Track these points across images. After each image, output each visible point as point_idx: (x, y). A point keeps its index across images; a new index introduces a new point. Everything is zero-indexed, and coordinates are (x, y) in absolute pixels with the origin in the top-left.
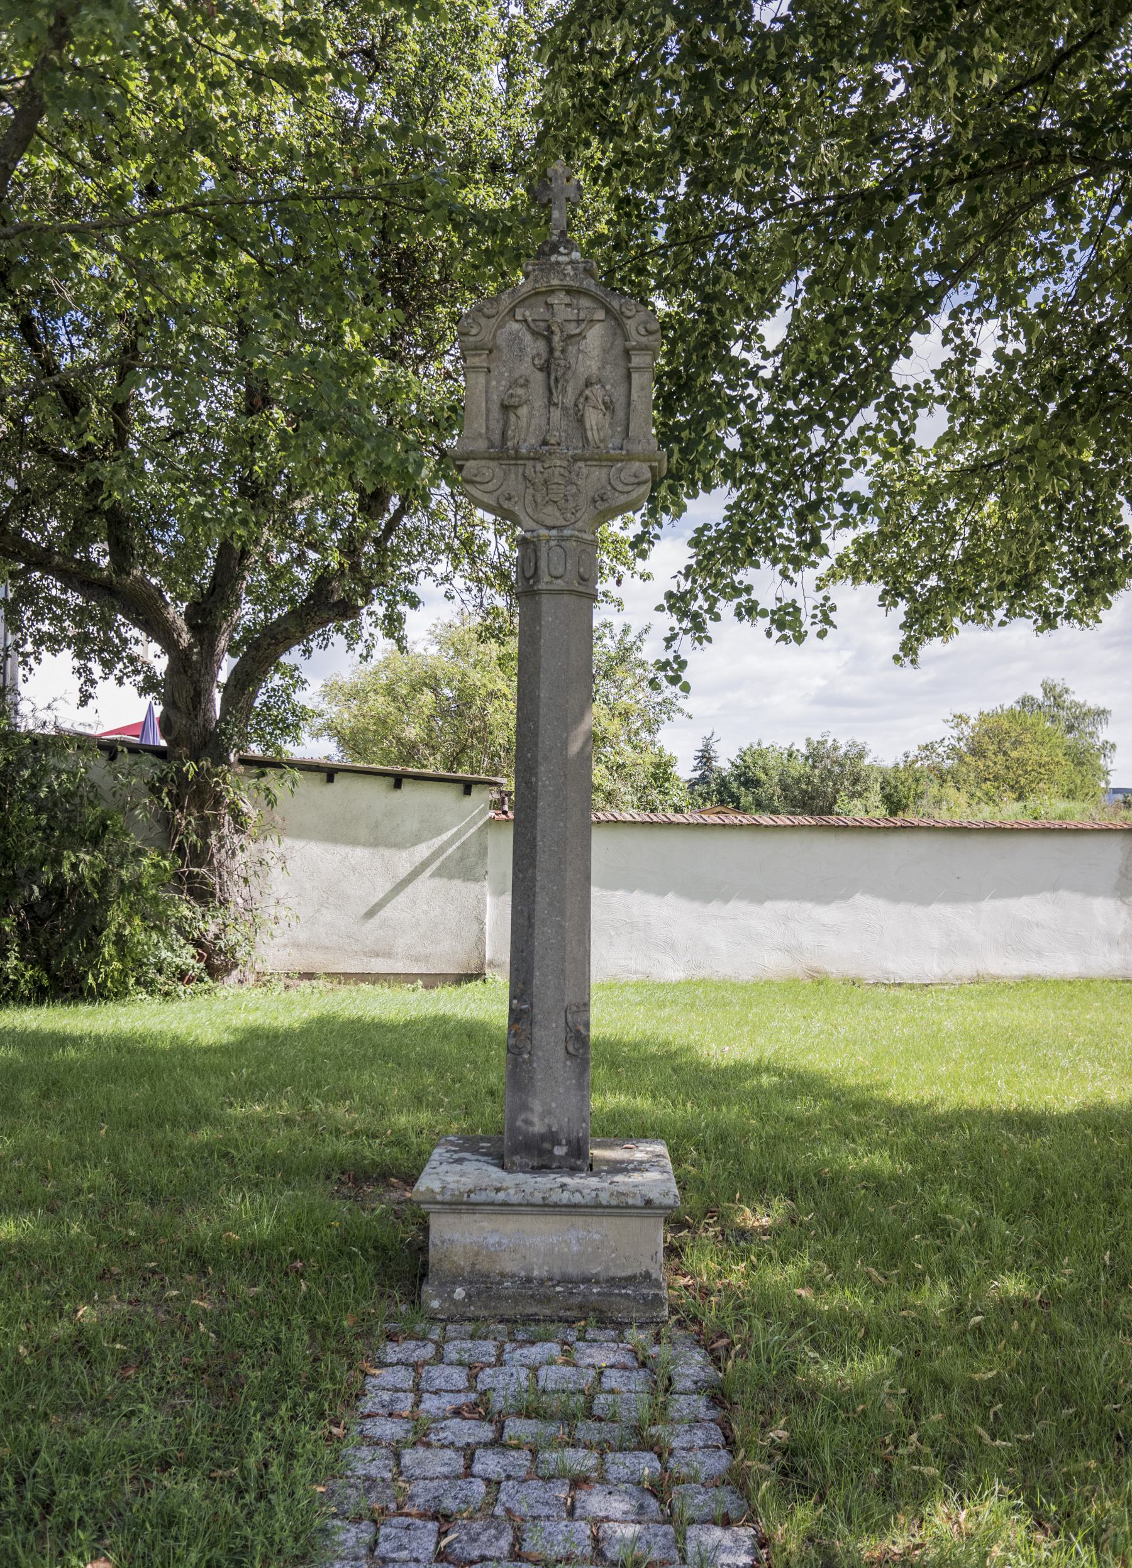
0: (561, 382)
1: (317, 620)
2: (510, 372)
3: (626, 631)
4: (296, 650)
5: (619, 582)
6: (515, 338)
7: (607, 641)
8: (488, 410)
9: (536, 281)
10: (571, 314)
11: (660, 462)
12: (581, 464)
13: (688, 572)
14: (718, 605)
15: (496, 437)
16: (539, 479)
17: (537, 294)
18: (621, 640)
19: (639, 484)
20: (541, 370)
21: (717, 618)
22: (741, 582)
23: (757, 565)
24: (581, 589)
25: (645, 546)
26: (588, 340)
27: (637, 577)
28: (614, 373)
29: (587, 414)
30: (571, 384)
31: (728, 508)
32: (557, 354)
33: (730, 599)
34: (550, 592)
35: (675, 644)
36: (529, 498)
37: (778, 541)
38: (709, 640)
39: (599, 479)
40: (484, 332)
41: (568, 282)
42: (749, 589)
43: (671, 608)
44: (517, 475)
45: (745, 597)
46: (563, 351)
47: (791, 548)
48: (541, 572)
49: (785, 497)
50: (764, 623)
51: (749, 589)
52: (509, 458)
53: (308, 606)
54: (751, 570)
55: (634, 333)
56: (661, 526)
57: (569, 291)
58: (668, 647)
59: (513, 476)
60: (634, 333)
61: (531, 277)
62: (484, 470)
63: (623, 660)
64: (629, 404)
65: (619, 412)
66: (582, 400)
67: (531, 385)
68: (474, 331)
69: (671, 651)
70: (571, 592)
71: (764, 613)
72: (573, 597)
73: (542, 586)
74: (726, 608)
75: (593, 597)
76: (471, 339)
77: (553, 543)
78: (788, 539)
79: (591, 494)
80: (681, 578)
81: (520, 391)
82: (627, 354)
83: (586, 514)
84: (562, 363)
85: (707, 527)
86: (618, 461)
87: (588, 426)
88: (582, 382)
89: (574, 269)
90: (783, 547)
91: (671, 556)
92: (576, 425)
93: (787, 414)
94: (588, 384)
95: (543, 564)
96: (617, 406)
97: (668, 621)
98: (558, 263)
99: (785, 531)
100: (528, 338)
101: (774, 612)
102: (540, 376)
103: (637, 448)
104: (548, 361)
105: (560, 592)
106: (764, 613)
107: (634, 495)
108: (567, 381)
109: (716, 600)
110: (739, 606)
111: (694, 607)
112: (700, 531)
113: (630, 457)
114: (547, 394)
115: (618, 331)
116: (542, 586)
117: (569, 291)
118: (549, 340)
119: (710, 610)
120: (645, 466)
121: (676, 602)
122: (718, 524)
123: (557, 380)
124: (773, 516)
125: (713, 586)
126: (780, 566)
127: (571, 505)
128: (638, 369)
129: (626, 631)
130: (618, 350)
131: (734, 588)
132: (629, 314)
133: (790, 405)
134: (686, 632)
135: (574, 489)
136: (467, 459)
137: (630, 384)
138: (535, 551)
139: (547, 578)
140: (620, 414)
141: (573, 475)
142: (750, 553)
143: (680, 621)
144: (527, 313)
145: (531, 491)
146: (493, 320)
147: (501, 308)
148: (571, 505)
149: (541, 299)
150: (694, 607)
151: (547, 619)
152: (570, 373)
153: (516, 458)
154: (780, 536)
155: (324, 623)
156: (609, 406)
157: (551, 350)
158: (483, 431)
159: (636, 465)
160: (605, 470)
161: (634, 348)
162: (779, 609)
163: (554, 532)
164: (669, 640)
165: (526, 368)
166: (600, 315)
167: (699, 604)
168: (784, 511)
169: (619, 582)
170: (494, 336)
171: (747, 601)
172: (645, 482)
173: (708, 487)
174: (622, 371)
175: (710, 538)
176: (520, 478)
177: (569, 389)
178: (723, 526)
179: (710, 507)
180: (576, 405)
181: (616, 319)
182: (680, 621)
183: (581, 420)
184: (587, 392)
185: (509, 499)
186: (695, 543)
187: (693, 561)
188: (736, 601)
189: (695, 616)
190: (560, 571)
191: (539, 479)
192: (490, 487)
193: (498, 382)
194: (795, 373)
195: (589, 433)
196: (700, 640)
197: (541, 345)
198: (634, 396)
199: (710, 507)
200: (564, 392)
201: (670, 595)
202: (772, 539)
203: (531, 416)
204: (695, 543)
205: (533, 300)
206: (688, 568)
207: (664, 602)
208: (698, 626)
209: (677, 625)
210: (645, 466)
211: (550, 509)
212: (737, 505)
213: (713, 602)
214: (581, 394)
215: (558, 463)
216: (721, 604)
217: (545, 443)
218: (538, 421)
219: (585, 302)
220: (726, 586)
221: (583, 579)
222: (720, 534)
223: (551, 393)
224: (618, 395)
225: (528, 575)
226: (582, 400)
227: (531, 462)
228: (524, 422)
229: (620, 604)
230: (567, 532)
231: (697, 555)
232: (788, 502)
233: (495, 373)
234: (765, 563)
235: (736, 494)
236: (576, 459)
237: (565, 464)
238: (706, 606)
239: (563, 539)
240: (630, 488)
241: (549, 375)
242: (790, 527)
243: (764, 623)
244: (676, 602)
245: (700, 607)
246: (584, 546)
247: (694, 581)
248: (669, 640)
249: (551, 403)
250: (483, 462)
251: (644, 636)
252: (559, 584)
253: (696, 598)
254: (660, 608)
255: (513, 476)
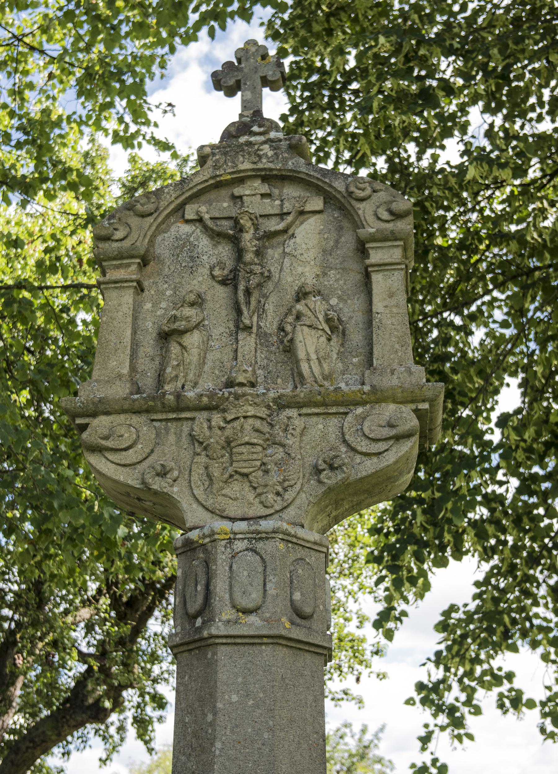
0: (255, 295)
1: (72, 723)
2: (175, 289)
3: (364, 731)
4: (57, 750)
5: (358, 680)
6: (184, 245)
7: (348, 739)
8: (135, 346)
9: (216, 167)
10: (270, 207)
11: (432, 401)
12: (293, 412)
13: (438, 659)
14: (476, 696)
15: (148, 382)
16: (216, 439)
17: (219, 185)
18: (360, 740)
19: (398, 438)
20: (223, 282)
21: (477, 711)
22: (500, 669)
23: (514, 649)
24: (296, 633)
25: (391, 625)
26: (298, 240)
27: (374, 676)
28: (340, 281)
29: (299, 337)
30: (273, 299)
31: (477, 584)
32: (249, 257)
33: (488, 687)
34: (234, 640)
35: (431, 746)
36: (198, 472)
37: (536, 622)
38: (470, 737)
39: (324, 436)
40: (134, 235)
41: (264, 164)
42: (510, 676)
43: (424, 702)
44: (179, 436)
45: (506, 686)
46: (258, 253)
47: (550, 630)
48: (216, 602)
49: (538, 573)
50: (533, 716)
51: (510, 676)
52: (166, 408)
53: (65, 709)
54: (509, 655)
55: (371, 219)
56: (407, 602)
57: (267, 177)
58: (423, 749)
59: (172, 438)
60: (371, 219)
61: (210, 163)
62: (122, 430)
63: (362, 757)
64: (369, 323)
65: (353, 334)
66: (290, 319)
67: (209, 305)
68: (119, 235)
69: (427, 753)
70: (277, 640)
71: (531, 704)
72: (282, 652)
73: (218, 628)
74: (486, 698)
75: (325, 653)
76: (115, 245)
77: (239, 545)
78: (545, 619)
79: (310, 460)
80: (431, 666)
81: (188, 311)
82: (362, 250)
83: (304, 496)
84: (257, 269)
85: (453, 608)
86: (357, 404)
87: (301, 354)
88: (290, 296)
89: (273, 148)
90: (541, 629)
91: (417, 641)
92: (283, 357)
93: (535, 478)
94: (301, 295)
95: (220, 586)
96: (351, 327)
97: (423, 716)
98: (250, 144)
99: (540, 610)
100: (204, 243)
101: (543, 704)
102: (221, 293)
103: (389, 382)
104: (235, 271)
105: (254, 640)
106: (531, 704)
107: (390, 458)
108: (266, 297)
109: (474, 690)
110: (501, 696)
111: (449, 698)
112: (447, 614)
113: (378, 397)
114: (233, 316)
115: (346, 224)
116: (218, 628)
117: (267, 177)
118: (235, 240)
119: (468, 702)
120: (407, 410)
121: (429, 694)
122: (466, 605)
123: (248, 292)
124: (527, 593)
125: (469, 674)
126: (540, 650)
127: (274, 478)
128: (382, 266)
129: (364, 731)
130: (348, 240)
131: (493, 675)
132: (361, 194)
133: (536, 469)
134: (443, 728)
135: (279, 453)
136: (94, 415)
137: (369, 293)
138: (207, 564)
139: (227, 614)
140: (356, 337)
141: (278, 430)
142: (506, 635)
143: (435, 716)
144: (203, 209)
145: (202, 459)
146: (150, 219)
147: (163, 204)
148: (274, 478)
149: (225, 193)
150: (449, 698)
151: (229, 698)
152: (270, 285)
153: (178, 409)
154: (537, 616)
155: (82, 724)
156: (335, 327)
157: (240, 253)
158: (125, 371)
159: (389, 410)
160: (334, 422)
161: (373, 239)
162: (549, 699)
163: (242, 526)
164: (425, 740)
165: (200, 282)
166: (317, 203)
167: (454, 695)
168: (538, 587)
169: (358, 680)
170: (152, 242)
171: (510, 690)
172: (408, 436)
173: (458, 554)
174: (355, 277)
175: (459, 620)
176: (185, 440)
177: (270, 307)
178: (472, 607)
179: (458, 581)
180: (281, 329)
181: (342, 208)
182: (435, 716)
183: (289, 350)
184: (300, 307)
185: (163, 473)
186: (443, 626)
187: (442, 647)
188: (496, 690)
189: (452, 710)
190: (253, 598)
191: (216, 439)
192: (131, 456)
193: (155, 305)
194: (539, 434)
195: (304, 367)
196: (459, 738)
197: (225, 251)
198: (378, 306)
199: (458, 581)
200: (261, 311)
201: (420, 687)
202: (529, 619)
203: (206, 349)
204: (443, 626)
205: (212, 195)
206: (438, 654)
207: (414, 694)
208: (457, 722)
209: (431, 721)
210: (407, 410)
211: (236, 488)
212: (486, 581)
213: (471, 692)
214: (289, 311)
215: (251, 411)
216: (480, 694)
217: (230, 384)
218: (219, 354)
219: (292, 192)
220: (484, 673)
221: (300, 615)
222: (470, 617)
223: (239, 312)
224: (352, 311)
225: (193, 608)
226: (290, 319)
227: (205, 414)
228: (193, 356)
229: (360, 701)
230: (266, 525)
231: (446, 640)
232: (541, 578)
233: (150, 292)
234: (524, 648)
235: (486, 567)
236: (282, 404)
237: (263, 412)
238: (463, 697)
239: (260, 536)
240: (382, 446)
241: (236, 288)
242: (546, 606)
243: (533, 716)
244: (429, 694)
245: (457, 699)
246: (301, 553)
247: (447, 669)
248: (425, 740)
249: (240, 327)
250: (122, 417)
251: (380, 735)
252: (253, 624)
253: (449, 688)
254: (410, 702)
255: (172, 438)
